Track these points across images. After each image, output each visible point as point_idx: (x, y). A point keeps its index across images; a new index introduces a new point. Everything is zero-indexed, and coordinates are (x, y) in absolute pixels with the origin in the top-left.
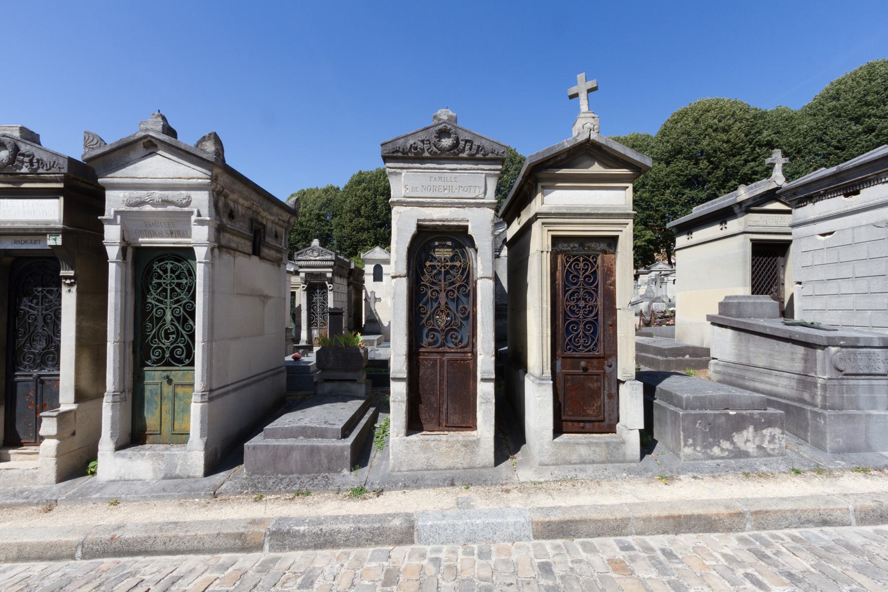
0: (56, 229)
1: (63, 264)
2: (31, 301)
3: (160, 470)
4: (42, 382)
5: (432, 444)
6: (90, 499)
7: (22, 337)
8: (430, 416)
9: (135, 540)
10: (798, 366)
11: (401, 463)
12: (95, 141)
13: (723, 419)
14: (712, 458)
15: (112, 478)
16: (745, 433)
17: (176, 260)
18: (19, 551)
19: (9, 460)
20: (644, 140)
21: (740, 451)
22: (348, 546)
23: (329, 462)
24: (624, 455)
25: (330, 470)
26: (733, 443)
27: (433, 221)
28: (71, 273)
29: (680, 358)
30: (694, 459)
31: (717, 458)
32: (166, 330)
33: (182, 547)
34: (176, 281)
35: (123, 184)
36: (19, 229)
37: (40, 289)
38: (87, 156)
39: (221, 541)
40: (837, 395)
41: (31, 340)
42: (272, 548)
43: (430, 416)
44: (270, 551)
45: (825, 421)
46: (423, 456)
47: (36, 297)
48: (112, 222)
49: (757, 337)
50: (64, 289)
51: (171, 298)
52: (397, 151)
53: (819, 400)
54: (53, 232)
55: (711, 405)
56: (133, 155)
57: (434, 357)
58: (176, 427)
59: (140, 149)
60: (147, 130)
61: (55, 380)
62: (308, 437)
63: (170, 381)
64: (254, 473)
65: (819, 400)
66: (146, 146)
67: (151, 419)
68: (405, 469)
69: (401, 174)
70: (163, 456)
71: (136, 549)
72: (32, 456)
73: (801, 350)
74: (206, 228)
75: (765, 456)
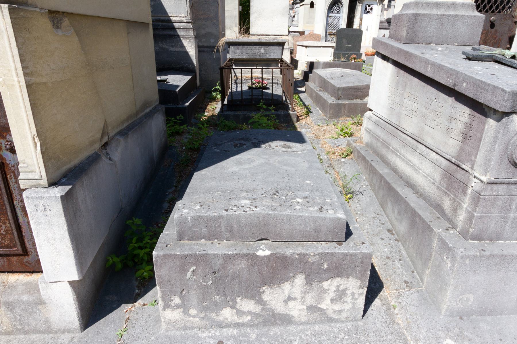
10: (451, 146)
13: (243, 264)
14: (221, 325)
16: (286, 287)
21: (274, 315)
24: (47, 321)
26: (260, 301)
29: (358, 101)
30: (185, 328)
31: (229, 325)
40: (496, 214)
45: (453, 265)
49: (416, 80)
53: (461, 217)
55: (231, 232)
65: (461, 217)
73: (464, 112)
75: (321, 322)
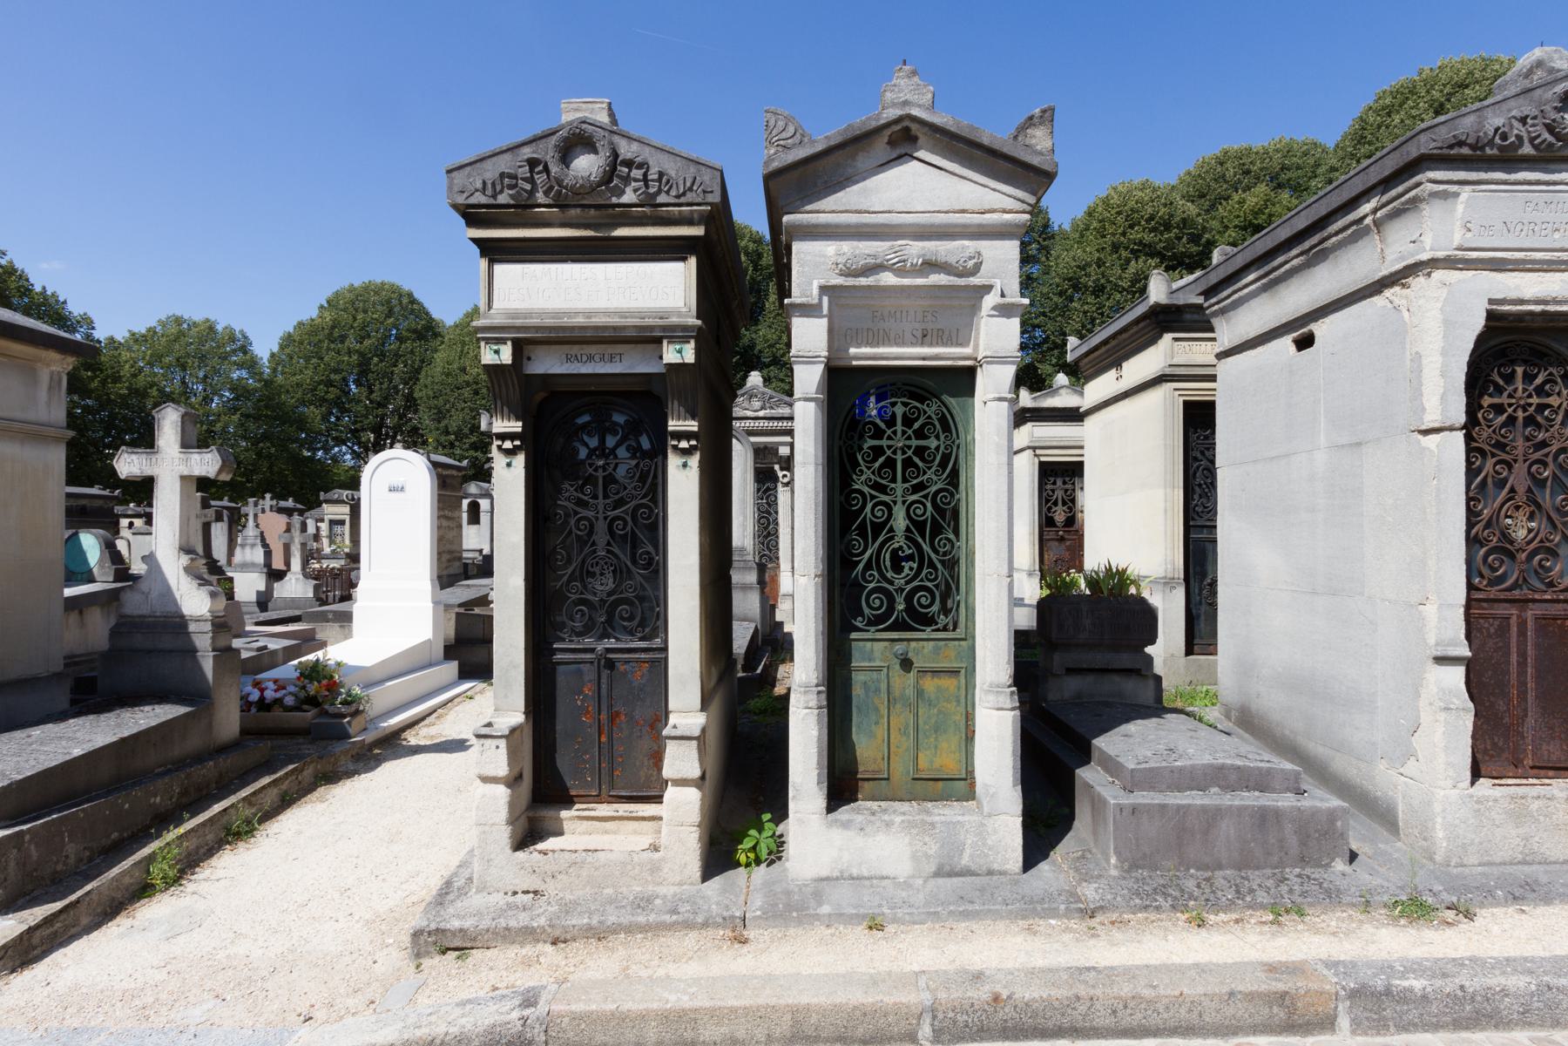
0: (685, 328)
1: (674, 406)
2: (581, 489)
3: (927, 856)
4: (611, 665)
5: (1535, 805)
6: (817, 917)
7: (565, 567)
8: (1494, 744)
9: (1048, 1003)
11: (1464, 846)
12: (791, 130)
15: (824, 873)
17: (913, 396)
18: (796, 1022)
19: (561, 833)
20: (1305, 154)
22: (1530, 1024)
23: (1303, 844)
25: (1303, 860)
27: (1522, 302)
28: (692, 426)
32: (894, 553)
33: (1155, 1020)
34: (914, 443)
35: (837, 226)
36: (605, 328)
37: (601, 463)
38: (776, 165)
39: (1239, 1010)
41: (584, 574)
42: (1357, 1027)
43: (1494, 744)
44: (1353, 1032)
46: (1514, 833)
47: (591, 480)
48: (808, 310)
50: (674, 461)
51: (905, 480)
52: (1461, 144)
54: (676, 334)
56: (863, 161)
57: (1501, 610)
58: (923, 763)
59: (880, 149)
60: (906, 103)
61: (658, 661)
62: (1228, 788)
63: (906, 664)
64: (1134, 866)
66: (892, 143)
67: (867, 748)
68: (1473, 860)
69: (1456, 195)
70: (933, 825)
71: (1050, 1024)
72: (608, 825)
74: (1015, 324)
